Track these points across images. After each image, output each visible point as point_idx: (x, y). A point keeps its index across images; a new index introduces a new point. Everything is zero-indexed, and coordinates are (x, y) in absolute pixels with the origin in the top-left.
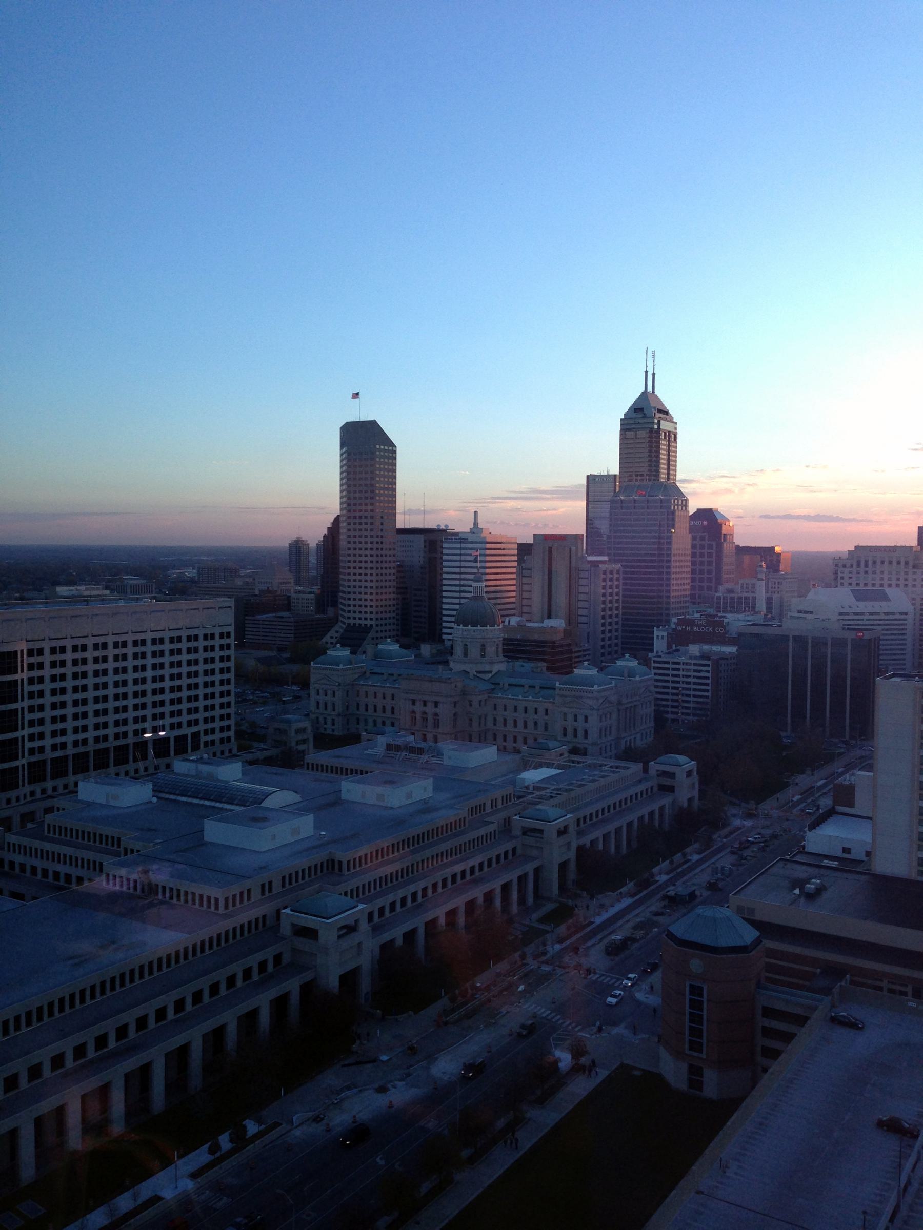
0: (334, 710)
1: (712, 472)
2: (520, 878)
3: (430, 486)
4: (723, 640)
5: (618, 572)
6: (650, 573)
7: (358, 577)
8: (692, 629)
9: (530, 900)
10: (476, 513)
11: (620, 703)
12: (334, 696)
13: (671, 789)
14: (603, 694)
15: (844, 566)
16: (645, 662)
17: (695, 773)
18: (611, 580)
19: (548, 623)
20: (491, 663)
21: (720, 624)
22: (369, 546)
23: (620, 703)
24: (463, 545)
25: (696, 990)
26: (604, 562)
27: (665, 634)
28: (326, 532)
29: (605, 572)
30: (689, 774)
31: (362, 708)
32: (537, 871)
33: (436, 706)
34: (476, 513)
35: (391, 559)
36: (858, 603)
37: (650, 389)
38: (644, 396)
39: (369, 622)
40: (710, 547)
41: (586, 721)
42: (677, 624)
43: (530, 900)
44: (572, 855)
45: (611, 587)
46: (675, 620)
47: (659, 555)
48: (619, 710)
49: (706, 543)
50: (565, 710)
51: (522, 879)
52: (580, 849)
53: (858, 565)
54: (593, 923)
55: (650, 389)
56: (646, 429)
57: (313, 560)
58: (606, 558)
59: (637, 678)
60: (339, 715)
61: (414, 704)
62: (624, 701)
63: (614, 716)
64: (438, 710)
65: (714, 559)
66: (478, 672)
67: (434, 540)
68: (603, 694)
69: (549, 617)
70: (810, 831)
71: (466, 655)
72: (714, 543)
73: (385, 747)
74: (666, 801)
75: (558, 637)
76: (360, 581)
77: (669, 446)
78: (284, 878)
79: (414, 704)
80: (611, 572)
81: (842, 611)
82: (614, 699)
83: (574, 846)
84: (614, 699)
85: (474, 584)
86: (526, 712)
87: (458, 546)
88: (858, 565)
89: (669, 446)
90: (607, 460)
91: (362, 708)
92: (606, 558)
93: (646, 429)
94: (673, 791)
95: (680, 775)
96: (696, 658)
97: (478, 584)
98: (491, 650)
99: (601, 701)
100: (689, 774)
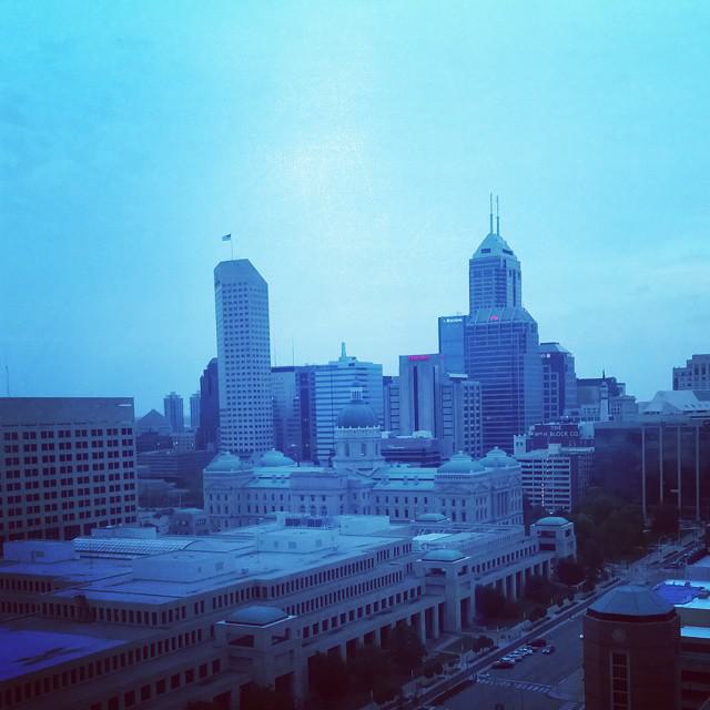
0: (227, 512)
1: (554, 308)
2: (426, 611)
3: (299, 337)
4: (579, 442)
5: (478, 388)
6: (506, 392)
7: (240, 353)
8: (549, 434)
9: (436, 632)
10: (343, 344)
11: (493, 489)
12: (226, 499)
13: (551, 548)
14: (478, 479)
15: (683, 374)
16: (510, 452)
17: (572, 533)
18: (472, 395)
19: (416, 435)
20: (372, 461)
21: (575, 428)
22: (242, 412)
23: (493, 489)
24: (333, 373)
25: (619, 659)
26: (465, 379)
27: (524, 442)
28: (202, 373)
29: (466, 388)
30: (568, 533)
31: (253, 509)
32: (441, 606)
33: (324, 499)
34: (343, 344)
35: (268, 394)
36: (701, 403)
37: (495, 232)
38: (493, 238)
39: (249, 448)
40: (554, 377)
41: (464, 505)
42: (534, 431)
43: (436, 632)
44: (471, 593)
45: (472, 402)
46: (532, 428)
47: (513, 364)
48: (492, 495)
49: (550, 373)
50: (444, 496)
51: (429, 612)
52: (479, 590)
53: (697, 372)
54: (497, 648)
55: (495, 232)
56: (494, 273)
57: (187, 412)
58: (466, 376)
59: (507, 467)
60: (232, 517)
61: (302, 499)
62: (497, 487)
63: (488, 499)
64: (325, 503)
65: (557, 396)
66: (360, 469)
67: (305, 377)
68: (478, 479)
69: (417, 429)
70: (689, 564)
71: (348, 454)
72: (557, 374)
73: (284, 523)
74: (548, 556)
75: (428, 446)
76: (238, 368)
77: (514, 282)
78: (196, 605)
79: (302, 499)
80: (472, 388)
81: (687, 409)
82: (488, 485)
83: (473, 586)
84: (488, 485)
85: (353, 389)
86: (406, 502)
87: (329, 373)
88: (697, 372)
89: (514, 282)
90: (458, 303)
91: (253, 509)
92: (466, 376)
93: (494, 273)
94: (554, 550)
95: (561, 536)
96: (556, 455)
97: (356, 389)
98: (370, 448)
99: (477, 485)
100: (568, 533)
